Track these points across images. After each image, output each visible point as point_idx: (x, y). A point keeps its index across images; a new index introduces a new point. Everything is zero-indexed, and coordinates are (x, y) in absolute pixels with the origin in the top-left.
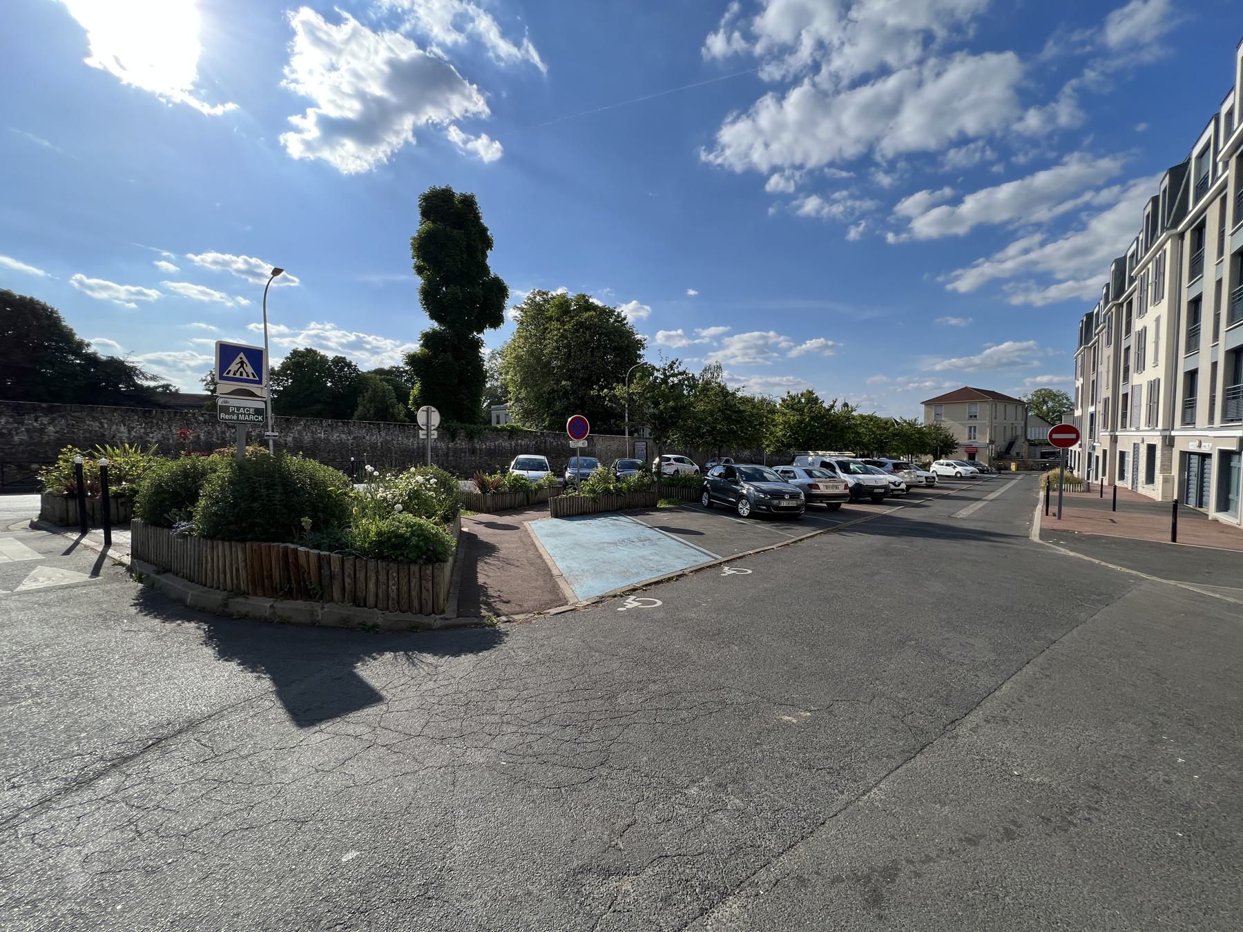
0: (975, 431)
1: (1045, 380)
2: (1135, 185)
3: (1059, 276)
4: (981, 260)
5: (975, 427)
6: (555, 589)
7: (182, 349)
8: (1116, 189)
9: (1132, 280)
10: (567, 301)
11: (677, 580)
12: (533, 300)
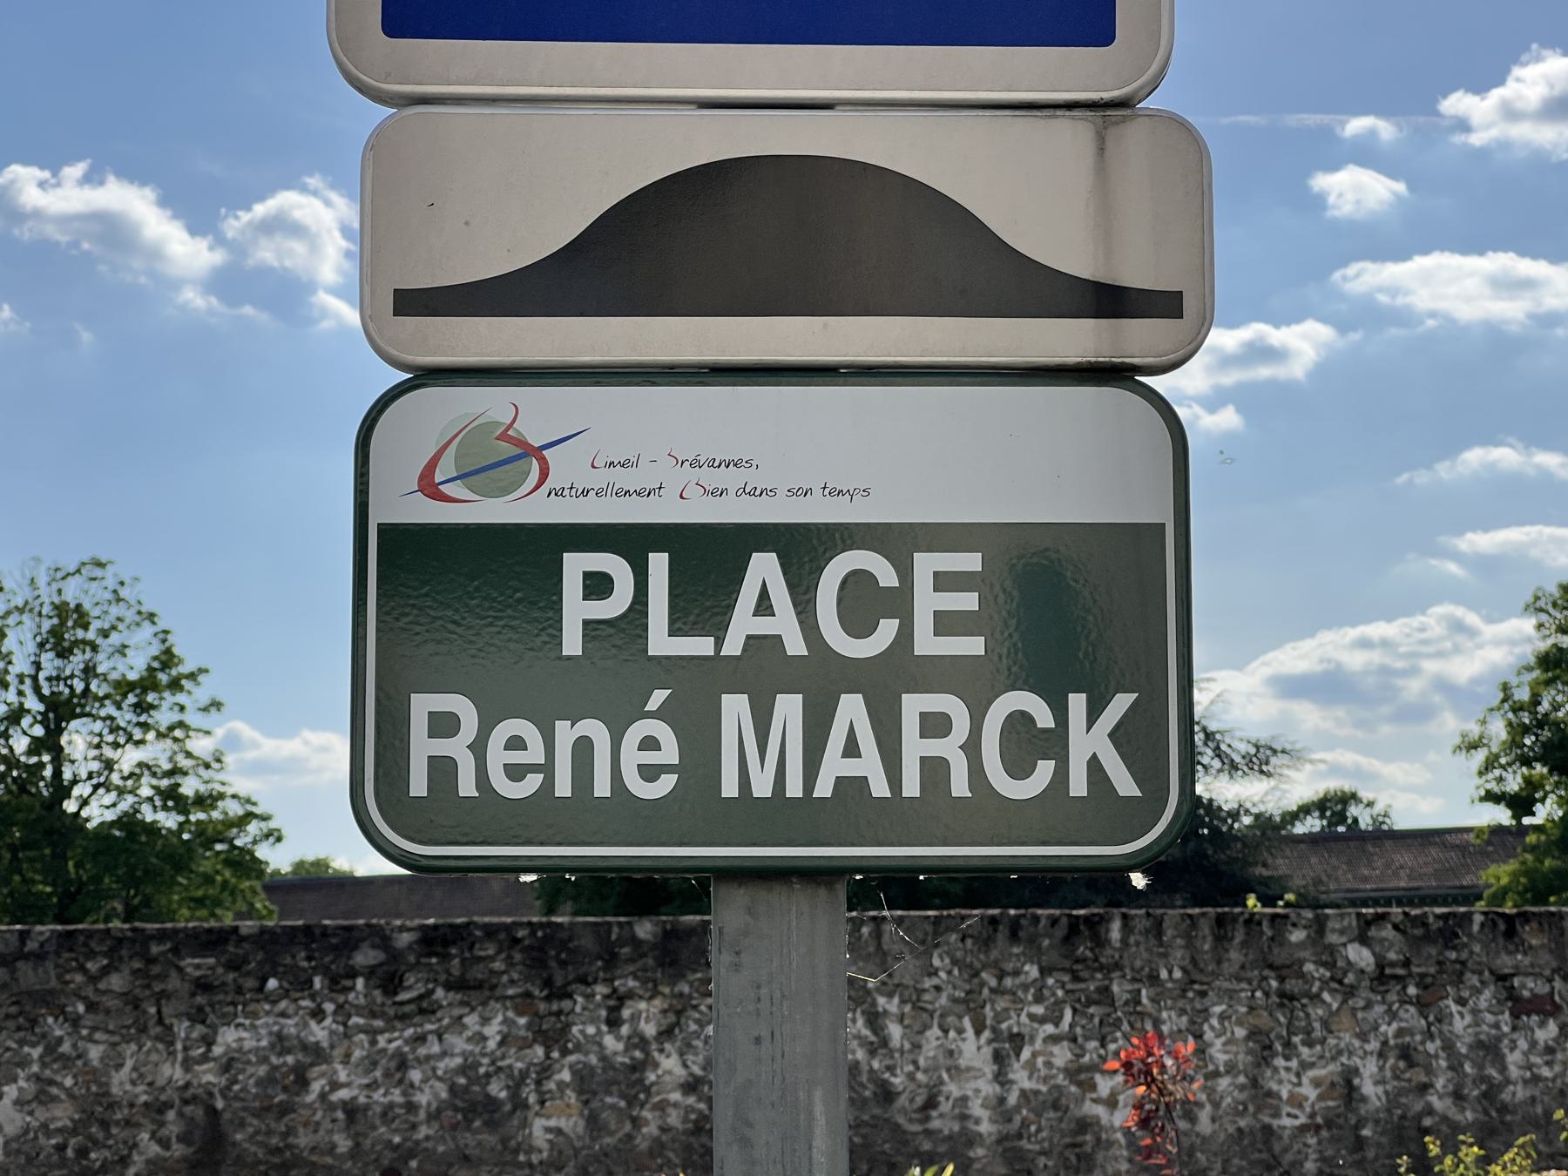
7: (1414, 602)
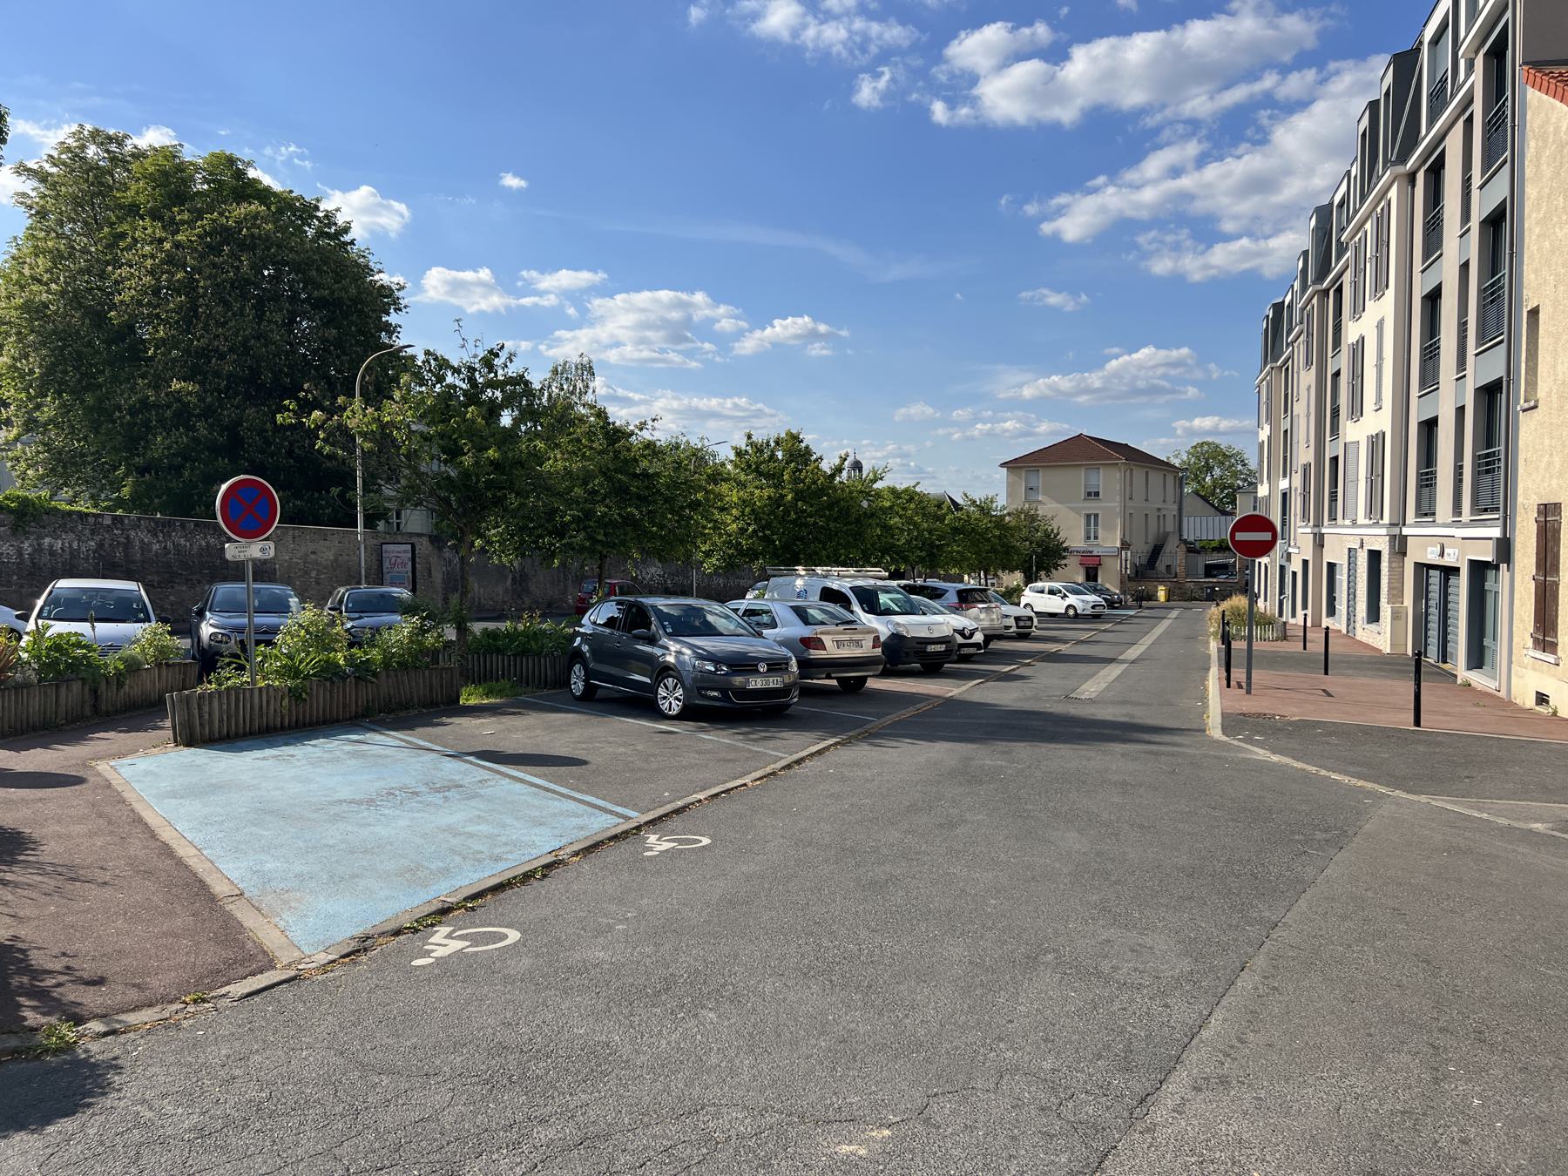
0: (1096, 524)
1: (1208, 427)
2: (1337, 73)
3: (1229, 227)
4: (1101, 180)
5: (1096, 516)
6: (230, 932)
8: (1310, 75)
9: (1342, 249)
10: (181, 167)
11: (544, 876)
12: (77, 155)
